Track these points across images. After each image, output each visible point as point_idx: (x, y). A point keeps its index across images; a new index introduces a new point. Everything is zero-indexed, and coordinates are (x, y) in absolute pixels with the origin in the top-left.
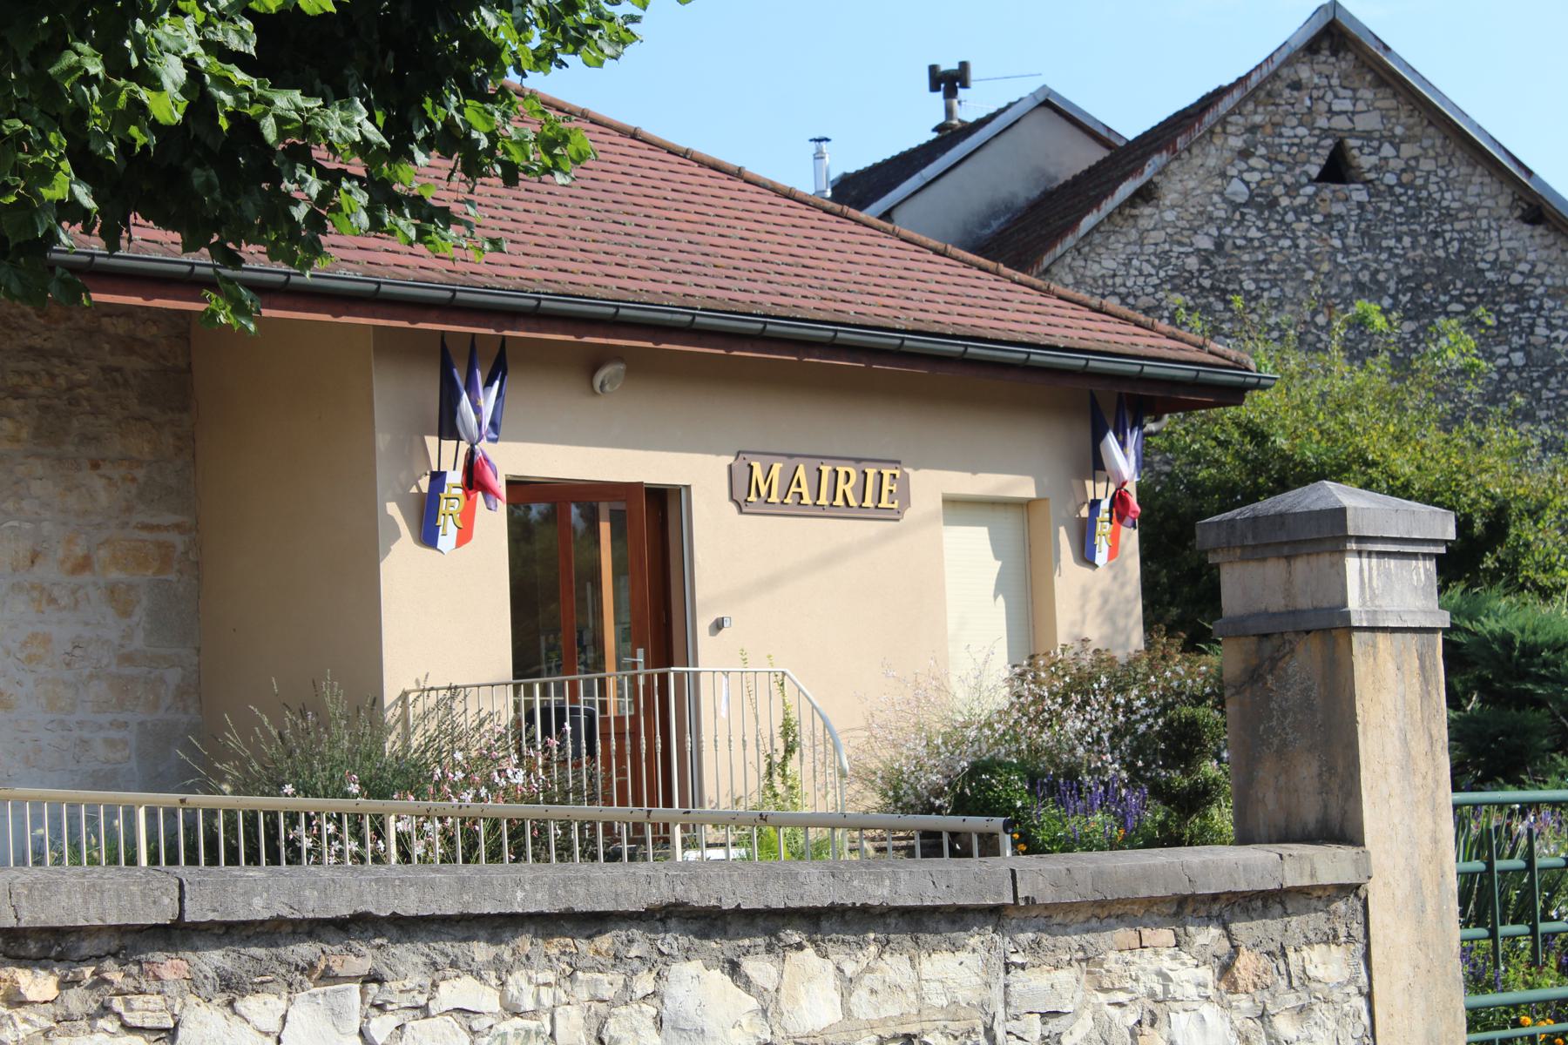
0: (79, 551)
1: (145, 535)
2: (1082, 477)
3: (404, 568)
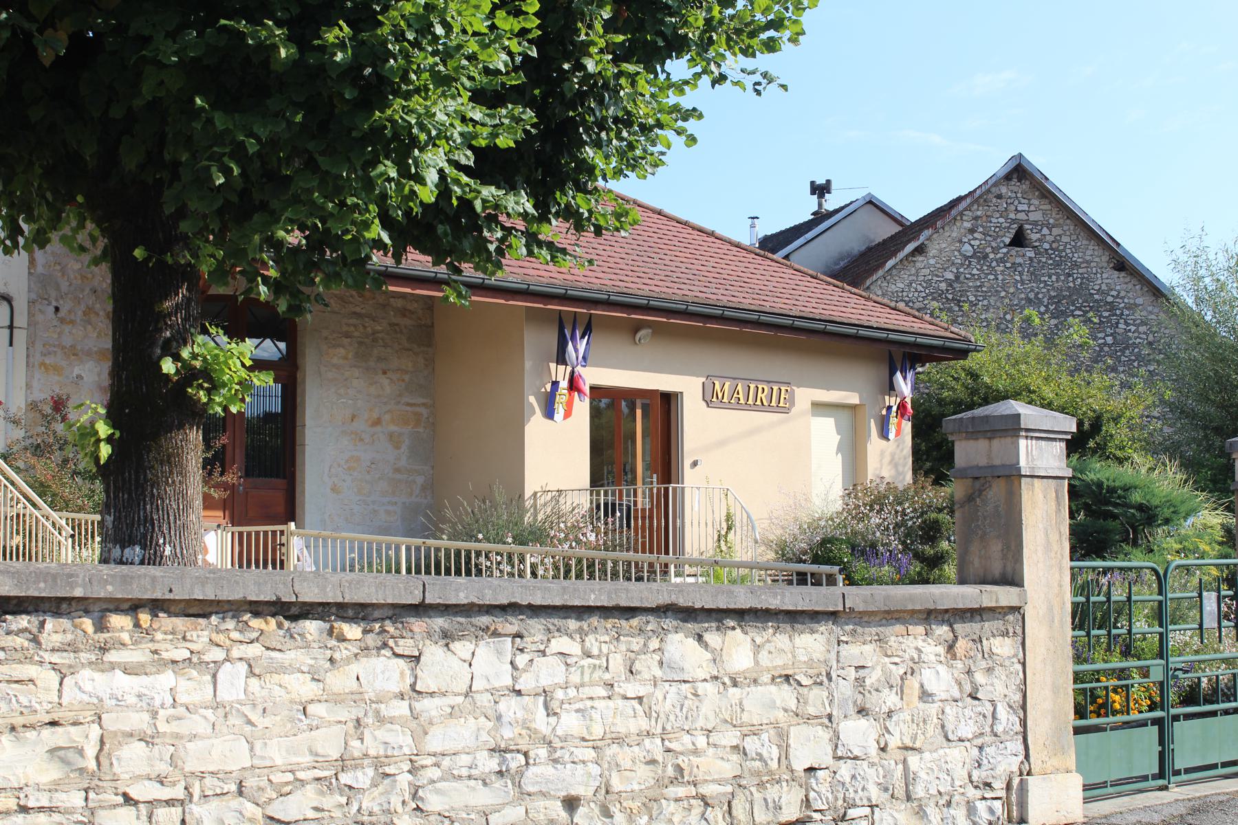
0: (375, 416)
1: (408, 408)
2: (884, 394)
3: (536, 428)
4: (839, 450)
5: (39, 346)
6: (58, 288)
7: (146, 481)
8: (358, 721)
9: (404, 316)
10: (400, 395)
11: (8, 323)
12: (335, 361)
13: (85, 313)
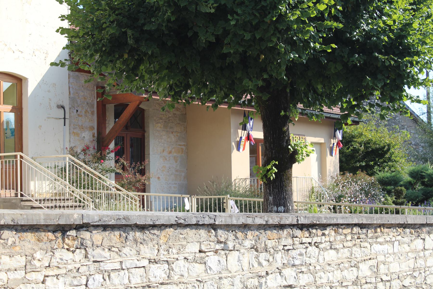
0: (170, 150)
1: (179, 147)
2: (331, 138)
3: (235, 154)
4: (317, 160)
5: (72, 125)
6: (77, 103)
7: (283, 185)
8: (415, 257)
9: (178, 111)
10: (177, 142)
11: (63, 117)
12: (158, 129)
13: (85, 113)
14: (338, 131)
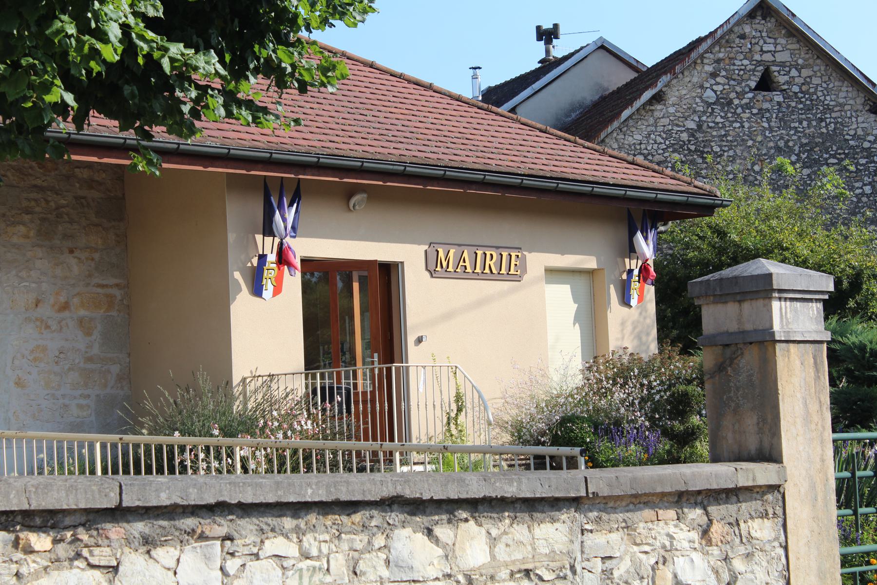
0: (62, 299)
1: (99, 290)
2: (623, 257)
3: (243, 307)
4: (577, 319)
10: (90, 276)
12: (15, 240)
14: (639, 235)
